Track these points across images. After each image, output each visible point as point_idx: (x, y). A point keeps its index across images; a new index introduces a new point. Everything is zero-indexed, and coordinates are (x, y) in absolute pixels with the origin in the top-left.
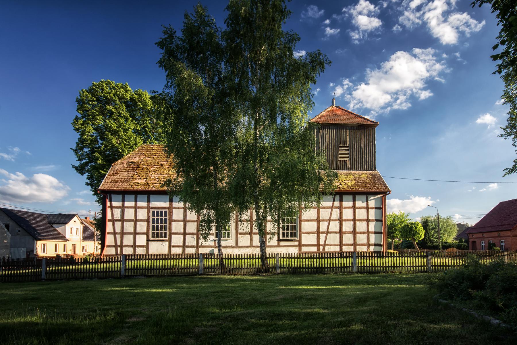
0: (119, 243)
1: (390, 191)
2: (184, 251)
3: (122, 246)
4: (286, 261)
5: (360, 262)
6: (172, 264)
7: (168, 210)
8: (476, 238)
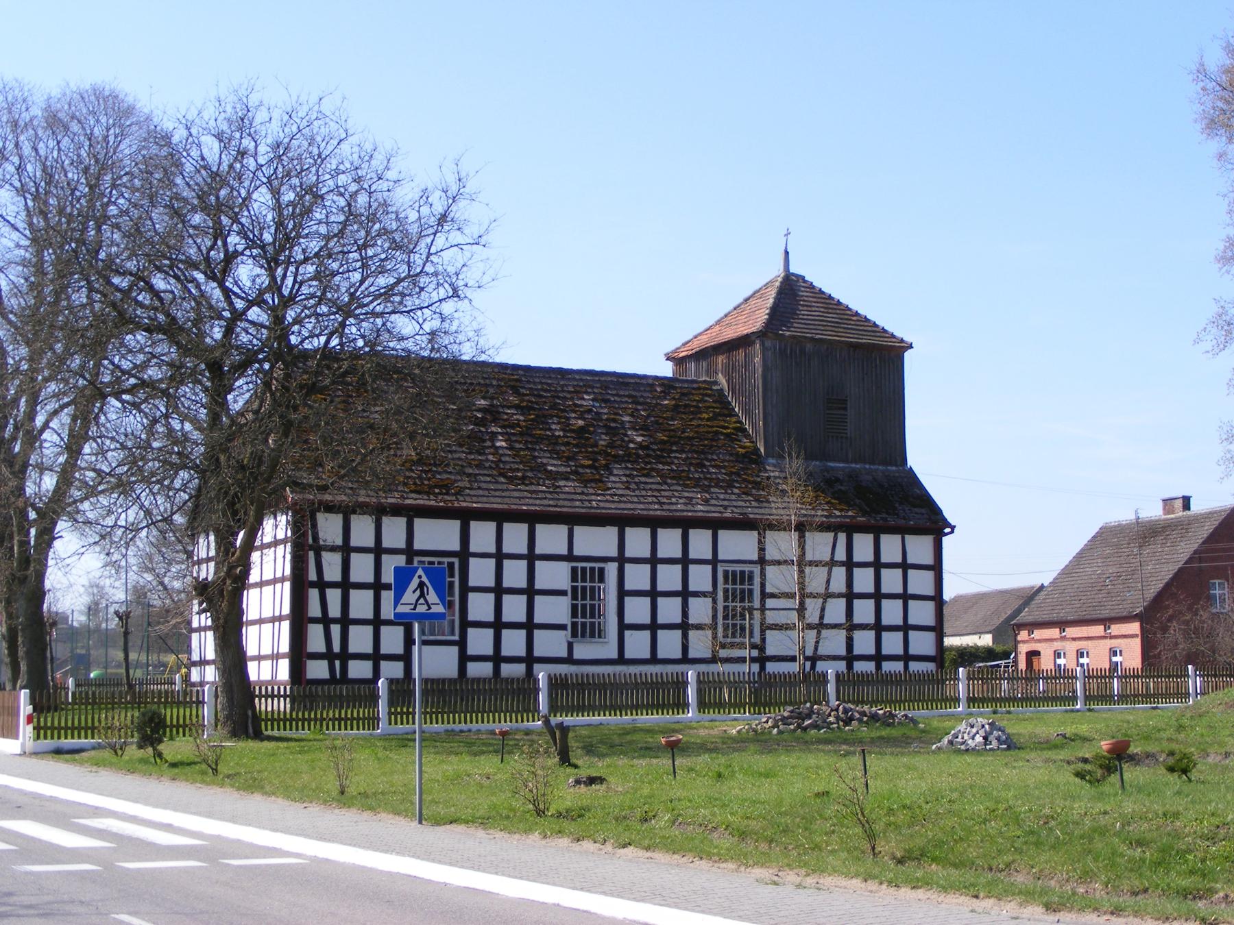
0: (337, 648)
1: (953, 528)
2: (497, 670)
3: (346, 656)
4: (100, 721)
5: (188, 714)
6: (282, 709)
7: (456, 561)
8: (1039, 641)
